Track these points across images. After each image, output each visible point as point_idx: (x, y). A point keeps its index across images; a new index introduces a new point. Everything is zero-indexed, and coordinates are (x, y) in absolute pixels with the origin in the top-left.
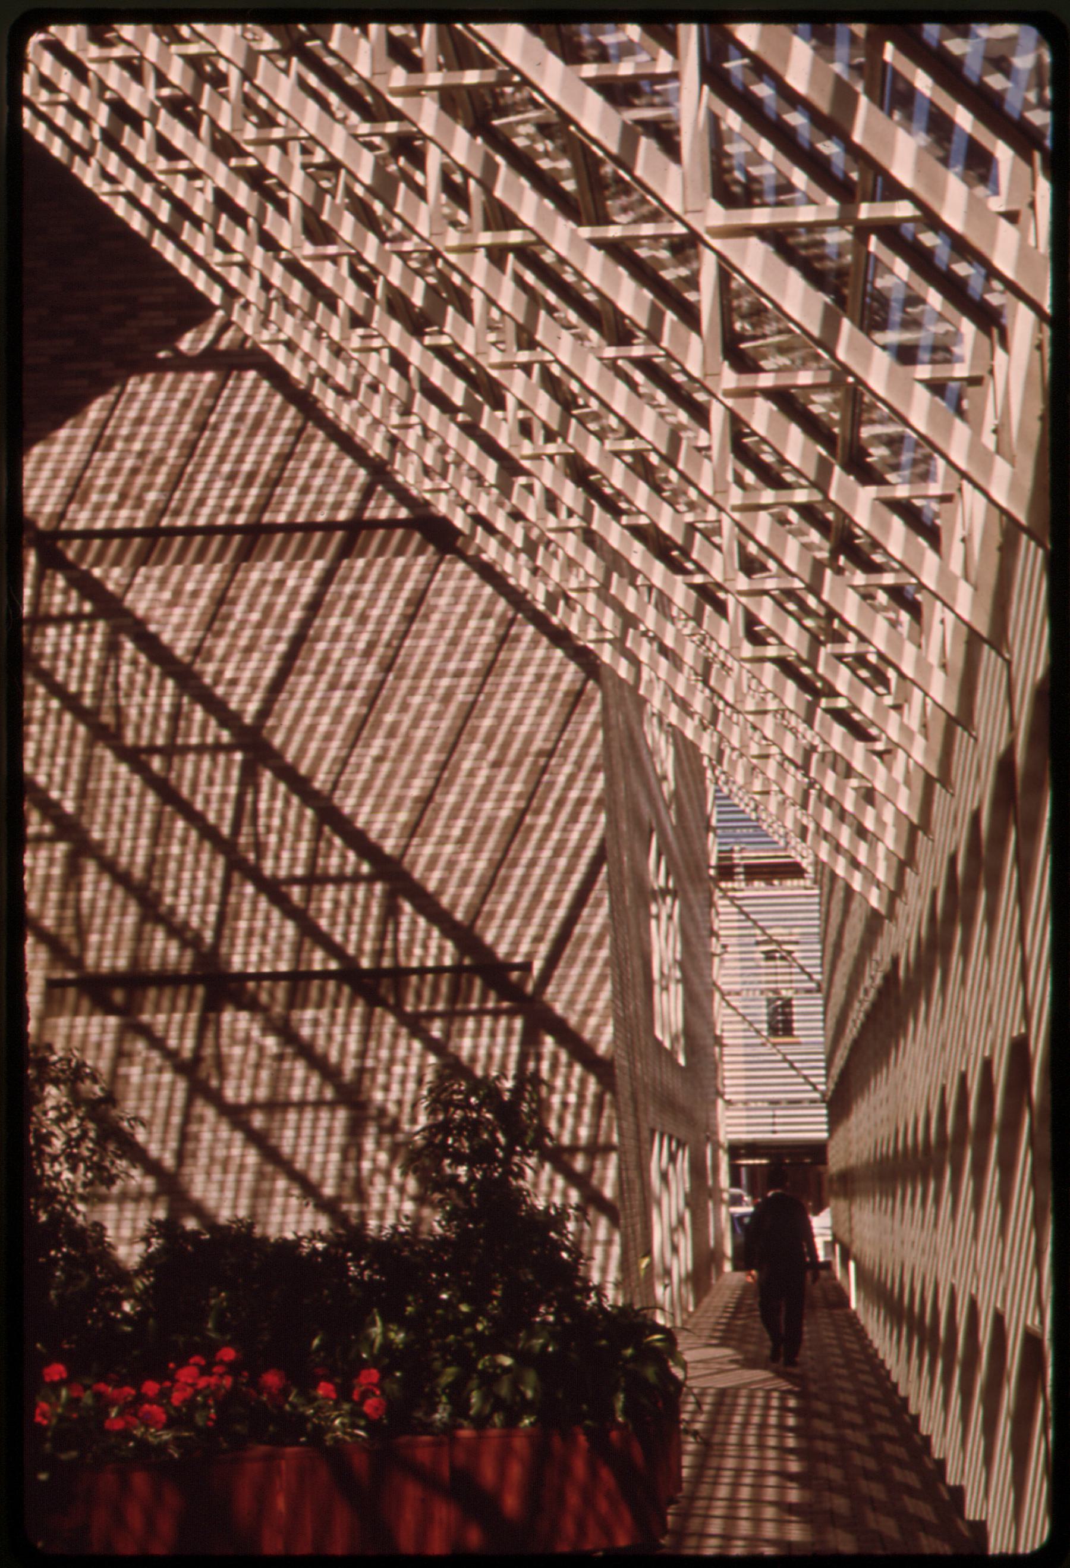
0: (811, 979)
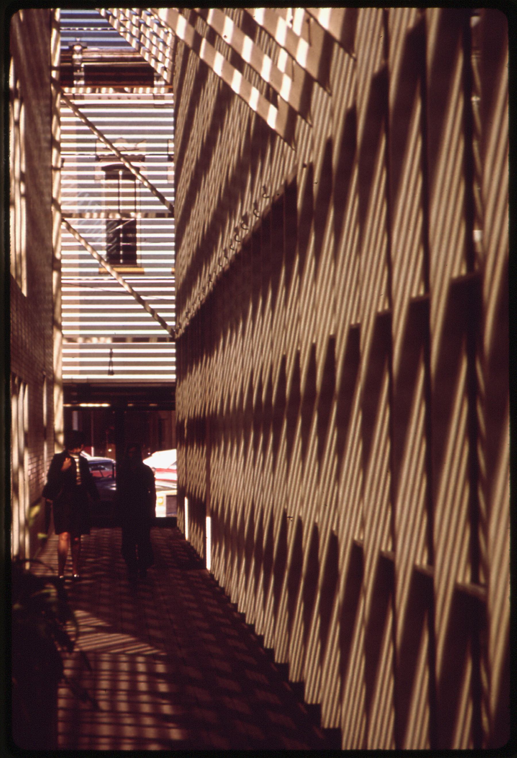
0: (163, 201)
